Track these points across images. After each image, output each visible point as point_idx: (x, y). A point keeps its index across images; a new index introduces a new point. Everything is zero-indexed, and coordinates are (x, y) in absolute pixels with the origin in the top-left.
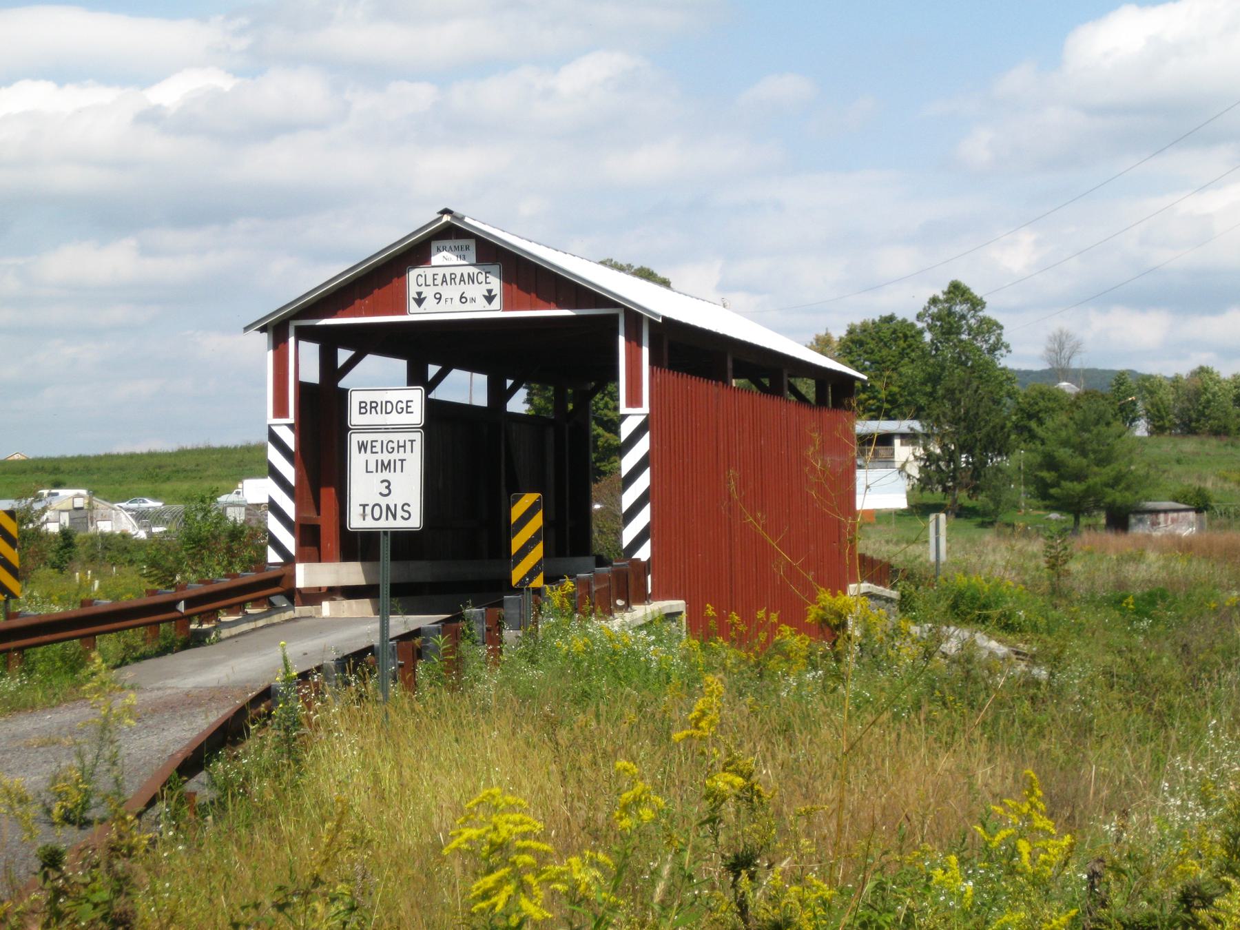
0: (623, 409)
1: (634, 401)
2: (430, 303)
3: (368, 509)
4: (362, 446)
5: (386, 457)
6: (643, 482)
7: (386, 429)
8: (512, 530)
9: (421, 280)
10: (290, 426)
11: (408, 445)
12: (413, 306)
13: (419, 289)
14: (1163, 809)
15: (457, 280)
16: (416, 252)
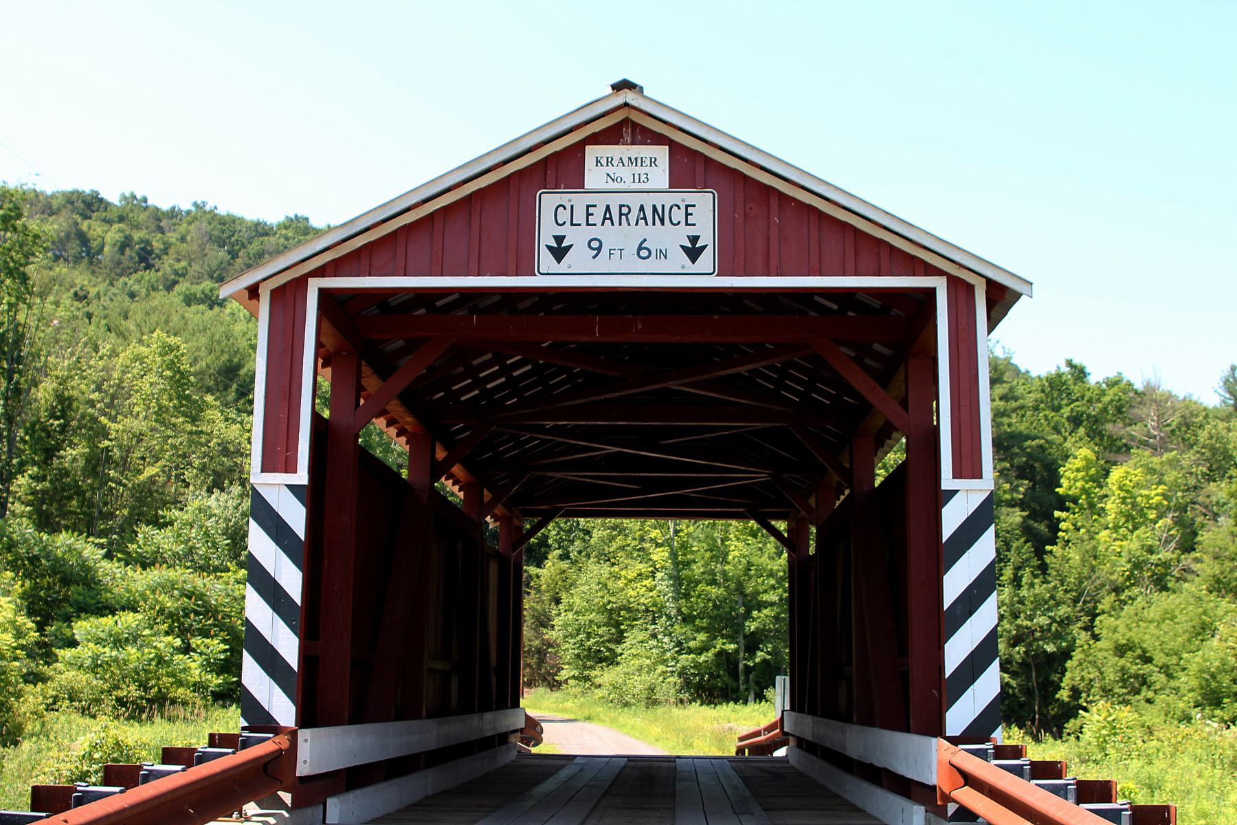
0: (947, 481)
1: (968, 467)
2: (578, 258)
6: (957, 650)
8: (944, 555)
9: (564, 216)
10: (293, 488)
12: (546, 260)
13: (560, 231)
14: (46, 602)
15: (633, 217)
16: (558, 163)
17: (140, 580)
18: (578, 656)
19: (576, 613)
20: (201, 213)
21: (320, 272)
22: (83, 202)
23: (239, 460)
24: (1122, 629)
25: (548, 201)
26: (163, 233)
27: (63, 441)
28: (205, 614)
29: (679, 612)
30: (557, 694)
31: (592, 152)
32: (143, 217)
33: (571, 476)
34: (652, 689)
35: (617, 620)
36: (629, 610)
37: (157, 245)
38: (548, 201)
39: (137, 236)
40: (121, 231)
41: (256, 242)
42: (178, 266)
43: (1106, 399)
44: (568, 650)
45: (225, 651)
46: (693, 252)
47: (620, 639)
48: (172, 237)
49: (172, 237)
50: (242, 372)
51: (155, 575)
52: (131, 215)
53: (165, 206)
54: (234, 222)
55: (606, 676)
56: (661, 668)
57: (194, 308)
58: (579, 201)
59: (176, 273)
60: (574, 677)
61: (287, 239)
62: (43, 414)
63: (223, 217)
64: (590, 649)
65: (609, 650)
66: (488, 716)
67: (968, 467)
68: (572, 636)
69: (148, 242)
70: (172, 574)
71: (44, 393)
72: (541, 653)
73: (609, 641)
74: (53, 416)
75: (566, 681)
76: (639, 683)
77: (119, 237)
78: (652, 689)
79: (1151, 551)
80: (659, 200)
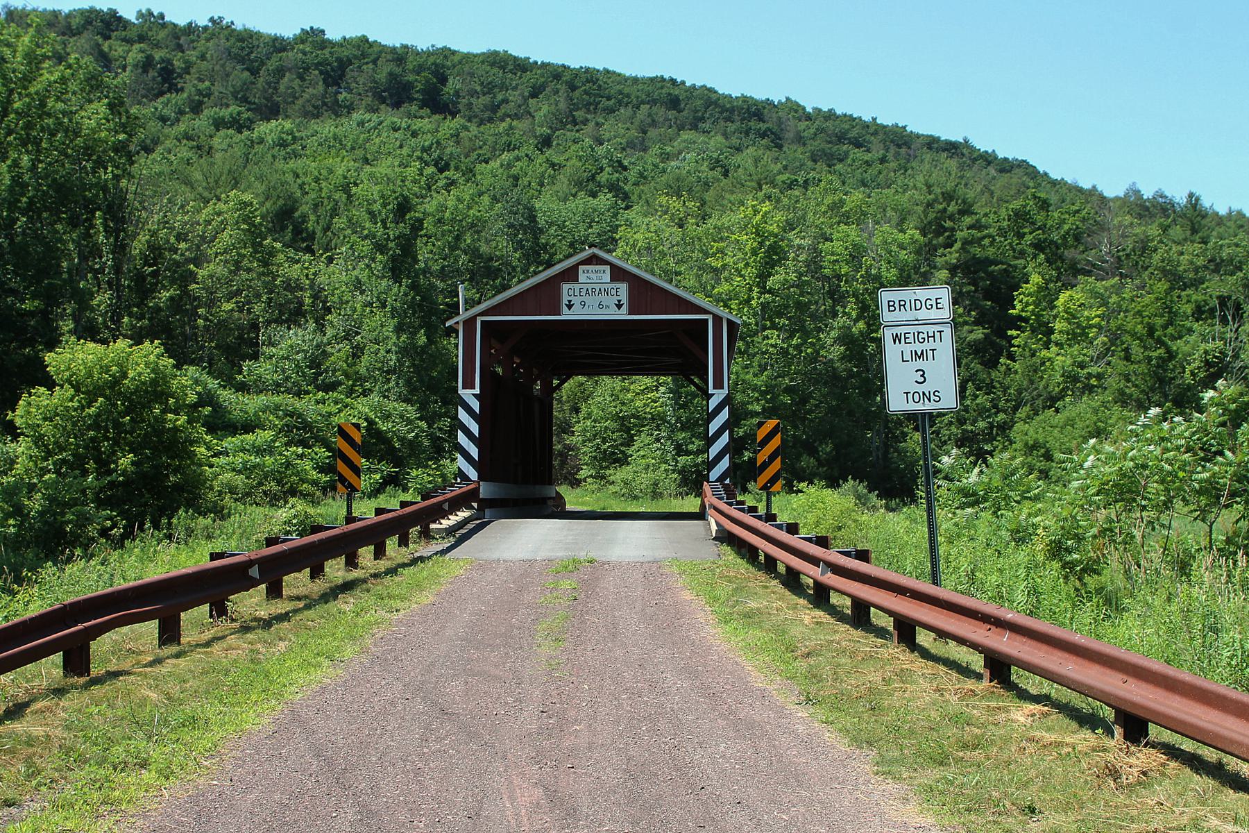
1: (718, 385)
3: (910, 396)
4: (896, 339)
5: (919, 348)
7: (917, 322)
9: (571, 292)
11: (937, 335)
12: (565, 309)
17: (251, 404)
18: (595, 458)
19: (595, 421)
20: (218, 28)
21: (482, 314)
22: (102, 21)
23: (299, 294)
24: (1031, 432)
25: (565, 287)
26: (183, 52)
27: (156, 284)
28: (304, 428)
29: (678, 419)
30: (578, 490)
31: (581, 268)
32: (162, 35)
33: (585, 353)
34: (656, 484)
35: (628, 426)
36: (637, 417)
37: (178, 64)
38: (565, 287)
39: (158, 55)
40: (142, 51)
41: (275, 58)
42: (201, 86)
43: (1066, 227)
44: (587, 452)
45: (329, 457)
46: (619, 306)
47: (629, 442)
48: (192, 55)
49: (192, 55)
50: (297, 214)
51: (262, 400)
52: (150, 34)
53: (182, 22)
54: (251, 37)
55: (618, 474)
56: (663, 466)
57: (222, 132)
58: (577, 286)
59: (200, 92)
60: (591, 476)
61: (305, 53)
62: (139, 263)
63: (240, 33)
64: (605, 451)
65: (623, 452)
66: (537, 487)
67: (718, 385)
68: (589, 440)
69: (169, 62)
70: (277, 399)
71: (138, 246)
72: (563, 456)
73: (622, 445)
74: (146, 263)
75: (585, 480)
76: (645, 480)
77: (140, 56)
78: (656, 484)
79: (1082, 366)
80: (606, 286)
